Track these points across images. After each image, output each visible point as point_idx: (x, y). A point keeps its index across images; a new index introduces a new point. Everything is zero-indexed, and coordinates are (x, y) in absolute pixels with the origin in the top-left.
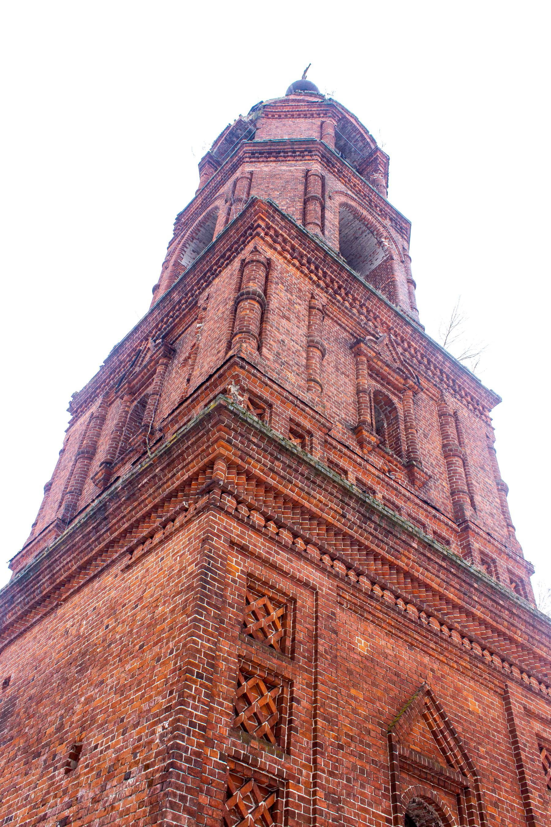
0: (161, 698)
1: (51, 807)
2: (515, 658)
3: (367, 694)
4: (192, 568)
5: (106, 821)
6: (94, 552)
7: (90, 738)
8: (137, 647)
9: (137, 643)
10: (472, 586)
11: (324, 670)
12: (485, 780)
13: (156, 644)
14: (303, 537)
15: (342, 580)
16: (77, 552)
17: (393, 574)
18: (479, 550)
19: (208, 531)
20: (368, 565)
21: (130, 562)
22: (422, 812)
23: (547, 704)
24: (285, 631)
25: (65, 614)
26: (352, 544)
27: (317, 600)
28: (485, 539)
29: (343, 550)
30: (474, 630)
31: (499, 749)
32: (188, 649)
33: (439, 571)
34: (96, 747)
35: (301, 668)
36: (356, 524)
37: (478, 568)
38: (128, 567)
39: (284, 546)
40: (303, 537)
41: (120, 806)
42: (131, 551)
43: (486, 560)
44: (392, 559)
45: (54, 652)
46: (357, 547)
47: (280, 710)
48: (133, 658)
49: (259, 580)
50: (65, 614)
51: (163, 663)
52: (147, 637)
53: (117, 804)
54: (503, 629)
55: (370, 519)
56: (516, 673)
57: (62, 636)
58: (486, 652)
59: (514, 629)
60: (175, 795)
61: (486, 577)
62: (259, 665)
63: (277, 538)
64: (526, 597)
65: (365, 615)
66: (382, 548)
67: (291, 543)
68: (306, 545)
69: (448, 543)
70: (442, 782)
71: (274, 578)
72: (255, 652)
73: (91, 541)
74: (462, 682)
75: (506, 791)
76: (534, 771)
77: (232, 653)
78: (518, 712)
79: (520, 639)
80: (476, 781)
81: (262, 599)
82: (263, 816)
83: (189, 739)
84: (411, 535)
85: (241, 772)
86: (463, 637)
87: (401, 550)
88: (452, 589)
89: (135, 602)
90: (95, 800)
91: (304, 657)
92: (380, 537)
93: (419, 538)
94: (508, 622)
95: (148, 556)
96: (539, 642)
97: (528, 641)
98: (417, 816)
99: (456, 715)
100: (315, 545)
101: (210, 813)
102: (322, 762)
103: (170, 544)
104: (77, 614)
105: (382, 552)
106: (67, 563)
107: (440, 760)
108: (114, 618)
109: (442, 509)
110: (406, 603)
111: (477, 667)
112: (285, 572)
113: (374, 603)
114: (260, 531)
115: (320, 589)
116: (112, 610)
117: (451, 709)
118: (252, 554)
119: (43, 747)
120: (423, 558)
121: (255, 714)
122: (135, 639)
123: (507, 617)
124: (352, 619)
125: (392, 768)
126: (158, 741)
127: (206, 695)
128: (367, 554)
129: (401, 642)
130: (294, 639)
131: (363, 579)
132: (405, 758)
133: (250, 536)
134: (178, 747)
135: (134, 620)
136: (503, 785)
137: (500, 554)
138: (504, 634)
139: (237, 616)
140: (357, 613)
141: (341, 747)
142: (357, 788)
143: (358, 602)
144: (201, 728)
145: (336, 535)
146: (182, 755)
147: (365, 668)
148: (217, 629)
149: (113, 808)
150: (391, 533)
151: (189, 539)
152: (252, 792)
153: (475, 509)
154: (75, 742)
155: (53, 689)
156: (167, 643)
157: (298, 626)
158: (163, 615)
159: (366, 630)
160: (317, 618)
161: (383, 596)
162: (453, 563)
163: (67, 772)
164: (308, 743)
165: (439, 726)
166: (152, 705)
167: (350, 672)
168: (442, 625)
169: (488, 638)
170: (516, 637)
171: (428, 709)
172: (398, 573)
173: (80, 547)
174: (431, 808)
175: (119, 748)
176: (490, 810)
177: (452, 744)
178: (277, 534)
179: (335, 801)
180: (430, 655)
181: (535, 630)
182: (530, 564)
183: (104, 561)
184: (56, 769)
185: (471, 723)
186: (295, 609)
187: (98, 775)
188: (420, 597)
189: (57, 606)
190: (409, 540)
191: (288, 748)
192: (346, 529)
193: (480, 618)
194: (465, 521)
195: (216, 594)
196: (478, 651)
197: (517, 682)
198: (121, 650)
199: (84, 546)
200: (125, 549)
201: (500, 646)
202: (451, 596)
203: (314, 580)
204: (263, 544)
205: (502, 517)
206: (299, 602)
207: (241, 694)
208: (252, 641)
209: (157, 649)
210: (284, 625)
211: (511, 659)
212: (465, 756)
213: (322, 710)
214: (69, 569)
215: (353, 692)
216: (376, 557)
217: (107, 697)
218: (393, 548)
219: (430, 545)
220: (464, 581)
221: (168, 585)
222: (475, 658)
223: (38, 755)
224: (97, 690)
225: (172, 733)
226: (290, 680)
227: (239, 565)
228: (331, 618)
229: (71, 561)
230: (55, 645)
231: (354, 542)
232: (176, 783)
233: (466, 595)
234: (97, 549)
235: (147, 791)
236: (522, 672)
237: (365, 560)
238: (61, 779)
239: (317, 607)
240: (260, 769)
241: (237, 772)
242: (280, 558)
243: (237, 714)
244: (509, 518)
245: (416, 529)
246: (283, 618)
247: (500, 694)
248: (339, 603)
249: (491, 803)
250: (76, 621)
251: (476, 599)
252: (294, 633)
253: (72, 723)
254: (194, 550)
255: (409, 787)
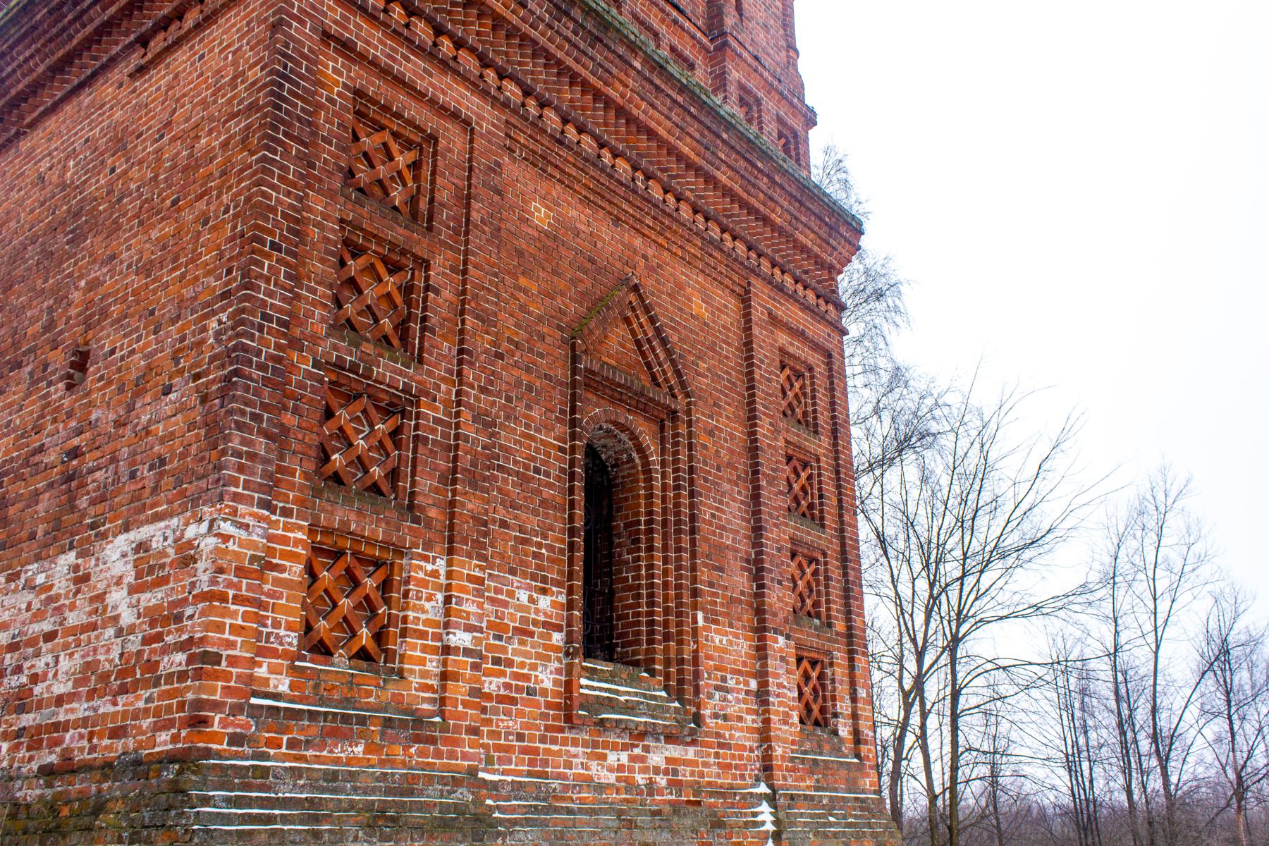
0: (212, 279)
1: (50, 435)
2: (768, 246)
3: (544, 285)
4: (255, 73)
5: (139, 450)
6: (75, 42)
7: (101, 339)
8: (168, 202)
9: (167, 197)
10: (719, 136)
11: (479, 248)
12: (701, 403)
13: (200, 197)
14: (451, 36)
15: (515, 111)
16: (42, 41)
17: (599, 109)
18: (739, 82)
19: (280, 10)
20: (559, 92)
21: (143, 61)
22: (610, 442)
23: (801, 310)
24: (419, 188)
25: (33, 149)
26: (534, 55)
27: (471, 141)
28: (750, 65)
29: (520, 64)
30: (714, 201)
31: (727, 366)
32: (255, 206)
33: (670, 110)
34: (113, 352)
35: (443, 243)
36: (543, 21)
37: (732, 109)
38: (141, 70)
39: (418, 47)
40: (451, 36)
41: (160, 429)
42: (144, 41)
43: (747, 101)
44: (599, 84)
45: (24, 211)
46: (542, 61)
47: (409, 303)
48: (162, 219)
49: (375, 102)
50: (33, 149)
51: (214, 228)
52: (183, 187)
53: (153, 427)
54: (757, 205)
55: (567, 14)
56: (765, 266)
57: (34, 185)
58: (726, 236)
59: (773, 205)
60: (243, 413)
61: (743, 125)
62: (375, 236)
63: (406, 32)
64: (798, 160)
65: (549, 170)
66: (583, 66)
67: (430, 43)
68: (457, 49)
69: (692, 67)
70: (642, 405)
71: (401, 100)
72: (369, 216)
73: (66, 20)
74: (687, 276)
75: (727, 417)
76: (768, 394)
77: (328, 215)
78: (760, 319)
79: (778, 220)
80: (689, 404)
81: (380, 134)
82: (380, 442)
83: (261, 338)
84: (633, 48)
85: (345, 386)
86: (696, 212)
87: (615, 71)
88: (688, 140)
89: (159, 130)
90: (119, 424)
91: (448, 227)
92: (582, 45)
93: (645, 53)
94: (766, 194)
95: (176, 51)
96: (805, 225)
97: (790, 223)
98: (604, 446)
99: (672, 320)
100: (472, 50)
101: (300, 436)
102: (469, 374)
103: (214, 32)
104: (56, 149)
105: (583, 72)
106: (26, 60)
107: (642, 377)
108: (124, 155)
109: (688, 12)
110: (615, 156)
111: (711, 255)
112: (420, 93)
113: (564, 153)
114: (376, 18)
115: (477, 123)
116: (120, 142)
117: (665, 311)
118: (362, 57)
119: (24, 354)
120: (648, 86)
121: (369, 307)
122: (164, 190)
123: (764, 187)
124: (528, 176)
125: (574, 384)
126: (212, 340)
127: (288, 276)
128: (559, 75)
129: (601, 213)
130: (432, 200)
131: (550, 114)
132: (592, 372)
133: (357, 26)
134: (245, 348)
135: (159, 160)
136: (725, 410)
137: (769, 92)
138: (757, 212)
139: (338, 157)
140: (536, 166)
141: (499, 356)
142: (521, 409)
143: (539, 149)
144: (284, 324)
145: (508, 37)
146: (251, 360)
147: (544, 248)
148: (302, 177)
149: (148, 433)
150: (601, 41)
151: (248, 24)
152: (364, 411)
153: (741, 15)
154: (78, 346)
155: (29, 269)
156: (218, 197)
157: (439, 180)
158: (209, 152)
159: (549, 193)
160: (471, 169)
161: (579, 142)
162: (694, 98)
163: (70, 387)
164: (450, 349)
165: (645, 333)
166: (200, 289)
167: (520, 253)
168: (666, 192)
169: (732, 215)
170: (773, 216)
171: (634, 310)
172: (606, 108)
173: (46, 32)
174: (623, 436)
175: (150, 353)
176: (703, 439)
177: (662, 356)
178: (407, 26)
179: (486, 423)
180: (644, 235)
181: (803, 209)
182: (812, 111)
183: (96, 58)
184: (50, 384)
185: (691, 331)
186: (435, 154)
187: (121, 390)
188: (637, 148)
189: (18, 135)
190: (629, 56)
191: (420, 355)
192: (525, 28)
193: (724, 186)
194: (723, 34)
195: (299, 119)
196: (715, 232)
197: (764, 279)
198: (141, 208)
199: (54, 31)
200: (132, 37)
201: (749, 228)
202: (686, 150)
203: (468, 108)
204: (380, 41)
205: (782, 32)
206: (443, 143)
207: (345, 277)
208: (363, 198)
209: (201, 205)
210: (416, 178)
211: (762, 246)
212: (678, 374)
213: (473, 304)
214: (32, 71)
215: (523, 281)
216: (574, 79)
217: (123, 279)
218: (602, 67)
219: (661, 67)
220: (708, 128)
221: (215, 102)
222: (710, 242)
223: (19, 365)
224: (105, 270)
225: (233, 329)
226: (424, 261)
227: (340, 74)
228: (494, 171)
229: (32, 56)
230: (24, 200)
231: (539, 52)
232: (244, 397)
233: (708, 149)
234: (80, 36)
235: (200, 408)
236: (773, 266)
237: (555, 83)
238: (61, 398)
239: (471, 153)
240: (376, 381)
241: (341, 385)
242: (411, 67)
243: (340, 306)
244: (793, 36)
245: (642, 37)
246: (415, 166)
247: (739, 295)
248: (509, 149)
249: (705, 430)
250: (55, 160)
251: (723, 157)
252: (432, 191)
253: (70, 318)
254: (258, 44)
255: (595, 411)
